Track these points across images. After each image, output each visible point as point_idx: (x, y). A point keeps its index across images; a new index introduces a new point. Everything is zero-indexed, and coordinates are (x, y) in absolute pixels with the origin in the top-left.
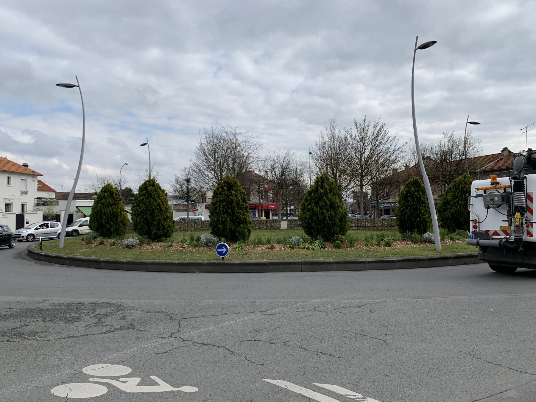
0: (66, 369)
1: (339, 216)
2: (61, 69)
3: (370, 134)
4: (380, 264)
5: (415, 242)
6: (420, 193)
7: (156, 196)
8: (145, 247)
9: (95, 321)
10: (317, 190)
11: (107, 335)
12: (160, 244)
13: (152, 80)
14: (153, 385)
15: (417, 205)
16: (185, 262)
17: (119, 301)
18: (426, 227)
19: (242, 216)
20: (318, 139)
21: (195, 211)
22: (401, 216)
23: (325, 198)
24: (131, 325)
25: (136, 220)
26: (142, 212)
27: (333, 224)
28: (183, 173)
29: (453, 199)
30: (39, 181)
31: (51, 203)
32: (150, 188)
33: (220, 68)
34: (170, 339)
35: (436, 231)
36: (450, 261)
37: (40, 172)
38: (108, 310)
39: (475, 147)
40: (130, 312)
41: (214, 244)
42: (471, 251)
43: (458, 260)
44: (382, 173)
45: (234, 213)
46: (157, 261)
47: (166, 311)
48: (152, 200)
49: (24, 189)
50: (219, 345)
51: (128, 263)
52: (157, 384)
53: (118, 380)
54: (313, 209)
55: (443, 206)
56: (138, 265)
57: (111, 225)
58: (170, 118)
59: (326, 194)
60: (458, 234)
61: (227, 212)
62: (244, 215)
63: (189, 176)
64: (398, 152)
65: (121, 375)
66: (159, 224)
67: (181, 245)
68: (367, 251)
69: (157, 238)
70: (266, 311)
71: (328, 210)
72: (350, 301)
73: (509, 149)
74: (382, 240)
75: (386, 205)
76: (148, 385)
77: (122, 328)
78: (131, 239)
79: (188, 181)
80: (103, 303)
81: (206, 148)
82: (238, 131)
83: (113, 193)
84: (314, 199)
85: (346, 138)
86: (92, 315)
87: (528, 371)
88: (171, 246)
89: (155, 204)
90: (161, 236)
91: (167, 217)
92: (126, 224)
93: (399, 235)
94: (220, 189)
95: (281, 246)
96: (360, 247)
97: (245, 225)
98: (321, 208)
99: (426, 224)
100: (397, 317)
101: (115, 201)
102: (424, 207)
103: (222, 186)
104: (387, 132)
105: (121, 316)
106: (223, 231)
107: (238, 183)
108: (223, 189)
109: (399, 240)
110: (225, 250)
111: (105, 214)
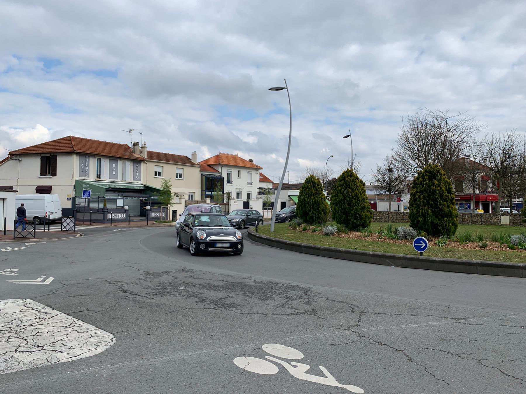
0: (250, 343)
2: (274, 76)
7: (353, 187)
8: (343, 235)
9: (283, 302)
11: (290, 317)
12: (357, 233)
13: (352, 75)
14: (320, 376)
16: (380, 253)
17: (308, 286)
19: (446, 209)
21: (399, 201)
24: (314, 311)
25: (335, 210)
26: (340, 201)
28: (386, 163)
30: (261, 174)
31: (269, 192)
32: (349, 179)
33: (422, 52)
34: (348, 332)
37: (261, 166)
38: (296, 293)
40: (315, 298)
41: (412, 237)
45: (436, 205)
46: (352, 250)
47: (350, 302)
48: (350, 190)
49: (249, 181)
50: (397, 348)
51: (325, 250)
52: (324, 376)
53: (290, 364)
56: (334, 253)
57: (313, 213)
58: (372, 109)
61: (428, 204)
62: (448, 207)
63: (392, 166)
65: (293, 359)
66: (356, 214)
67: (378, 235)
69: (355, 228)
70: (462, 319)
76: (316, 375)
77: (305, 313)
78: (330, 227)
79: (390, 170)
80: (294, 286)
81: (409, 136)
82: (449, 115)
83: (315, 183)
86: (283, 296)
88: (368, 236)
89: (353, 194)
90: (359, 225)
91: (364, 207)
92: (326, 212)
94: (420, 179)
95: (496, 244)
97: (450, 219)
101: (317, 191)
103: (423, 175)
105: (307, 300)
106: (424, 224)
107: (442, 172)
108: (424, 178)
110: (424, 245)
111: (308, 203)
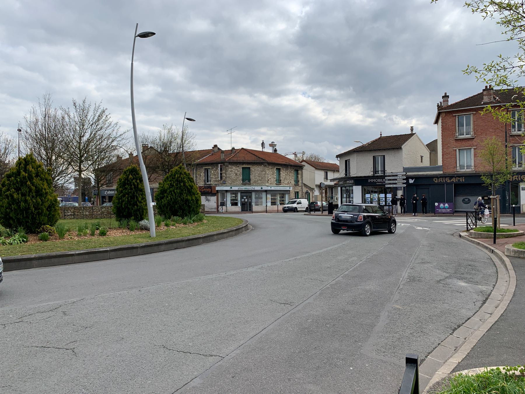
1: (47, 204)
3: (90, 116)
4: (91, 256)
5: (131, 229)
6: (138, 181)
10: (19, 173)
15: (134, 193)
18: (143, 214)
20: (28, 116)
22: (118, 203)
23: (29, 183)
27: (39, 214)
29: (170, 188)
35: (151, 220)
36: (163, 247)
39: (190, 141)
42: (182, 236)
43: (170, 245)
44: (103, 159)
54: (12, 196)
55: (160, 194)
59: (30, 178)
60: (173, 221)
64: (119, 139)
68: (79, 242)
71: (33, 197)
72: (41, 305)
73: (218, 147)
74: (97, 229)
75: (109, 192)
84: (14, 184)
85: (63, 118)
87: (213, 353)
93: (116, 224)
96: (71, 238)
98: (23, 195)
99: (143, 212)
100: (95, 316)
102: (142, 195)
104: (108, 117)
109: (115, 228)
